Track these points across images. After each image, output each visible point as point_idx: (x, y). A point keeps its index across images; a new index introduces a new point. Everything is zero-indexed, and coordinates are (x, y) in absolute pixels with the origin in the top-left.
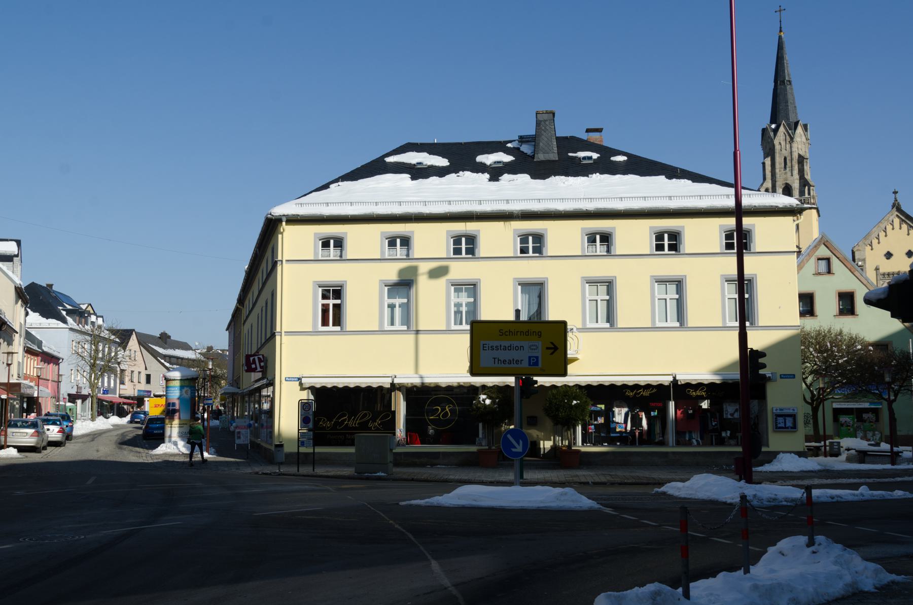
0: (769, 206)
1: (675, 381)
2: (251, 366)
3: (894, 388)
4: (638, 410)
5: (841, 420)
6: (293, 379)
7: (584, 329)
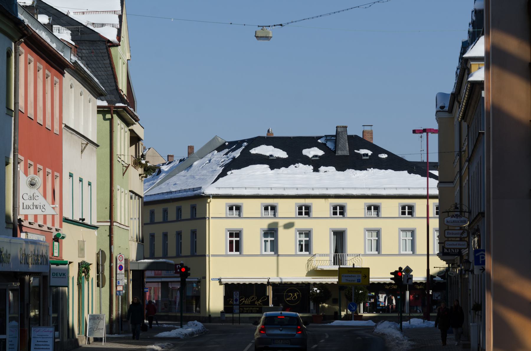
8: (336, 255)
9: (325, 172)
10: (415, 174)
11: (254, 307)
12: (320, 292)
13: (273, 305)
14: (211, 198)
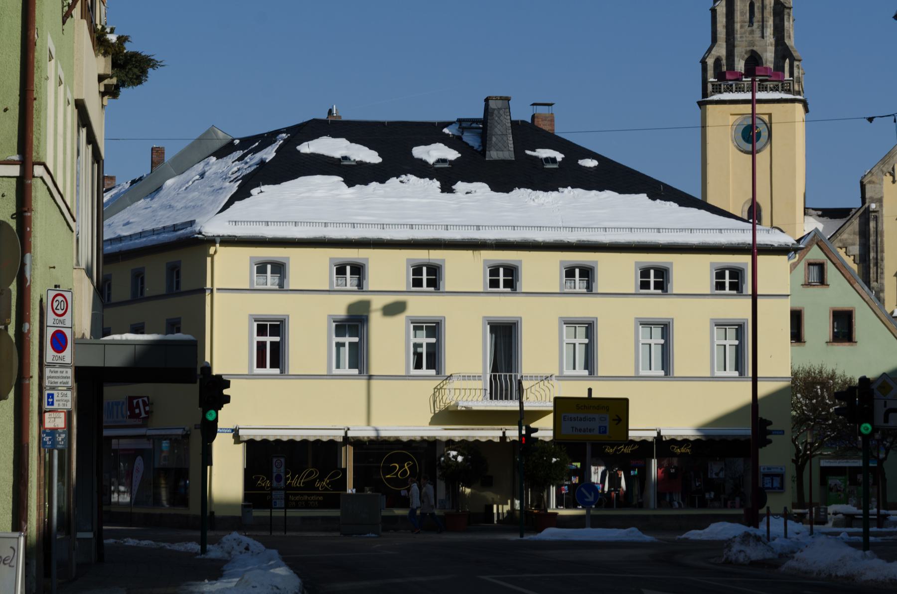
0: (764, 245)
1: (659, 437)
2: (135, 411)
3: (886, 445)
4: (617, 469)
5: (830, 482)
6: (226, 431)
7: (561, 377)
8: (495, 376)
9: (467, 193)
10: (665, 201)
11: (313, 494)
12: (463, 460)
13: (354, 491)
14: (218, 245)
